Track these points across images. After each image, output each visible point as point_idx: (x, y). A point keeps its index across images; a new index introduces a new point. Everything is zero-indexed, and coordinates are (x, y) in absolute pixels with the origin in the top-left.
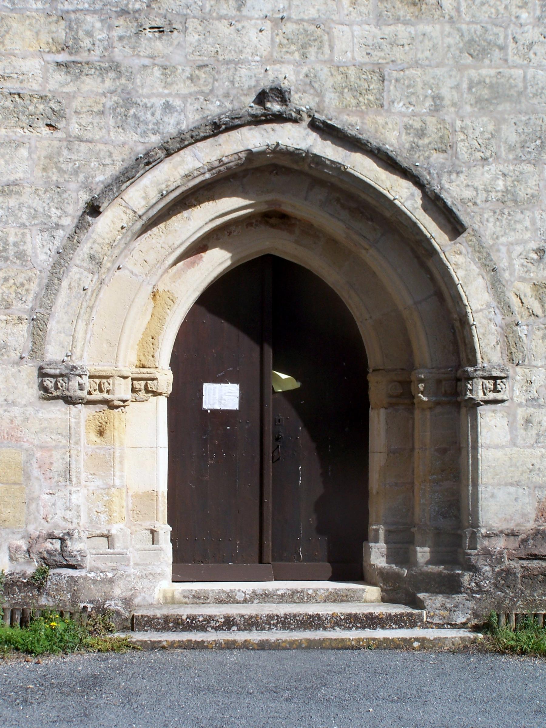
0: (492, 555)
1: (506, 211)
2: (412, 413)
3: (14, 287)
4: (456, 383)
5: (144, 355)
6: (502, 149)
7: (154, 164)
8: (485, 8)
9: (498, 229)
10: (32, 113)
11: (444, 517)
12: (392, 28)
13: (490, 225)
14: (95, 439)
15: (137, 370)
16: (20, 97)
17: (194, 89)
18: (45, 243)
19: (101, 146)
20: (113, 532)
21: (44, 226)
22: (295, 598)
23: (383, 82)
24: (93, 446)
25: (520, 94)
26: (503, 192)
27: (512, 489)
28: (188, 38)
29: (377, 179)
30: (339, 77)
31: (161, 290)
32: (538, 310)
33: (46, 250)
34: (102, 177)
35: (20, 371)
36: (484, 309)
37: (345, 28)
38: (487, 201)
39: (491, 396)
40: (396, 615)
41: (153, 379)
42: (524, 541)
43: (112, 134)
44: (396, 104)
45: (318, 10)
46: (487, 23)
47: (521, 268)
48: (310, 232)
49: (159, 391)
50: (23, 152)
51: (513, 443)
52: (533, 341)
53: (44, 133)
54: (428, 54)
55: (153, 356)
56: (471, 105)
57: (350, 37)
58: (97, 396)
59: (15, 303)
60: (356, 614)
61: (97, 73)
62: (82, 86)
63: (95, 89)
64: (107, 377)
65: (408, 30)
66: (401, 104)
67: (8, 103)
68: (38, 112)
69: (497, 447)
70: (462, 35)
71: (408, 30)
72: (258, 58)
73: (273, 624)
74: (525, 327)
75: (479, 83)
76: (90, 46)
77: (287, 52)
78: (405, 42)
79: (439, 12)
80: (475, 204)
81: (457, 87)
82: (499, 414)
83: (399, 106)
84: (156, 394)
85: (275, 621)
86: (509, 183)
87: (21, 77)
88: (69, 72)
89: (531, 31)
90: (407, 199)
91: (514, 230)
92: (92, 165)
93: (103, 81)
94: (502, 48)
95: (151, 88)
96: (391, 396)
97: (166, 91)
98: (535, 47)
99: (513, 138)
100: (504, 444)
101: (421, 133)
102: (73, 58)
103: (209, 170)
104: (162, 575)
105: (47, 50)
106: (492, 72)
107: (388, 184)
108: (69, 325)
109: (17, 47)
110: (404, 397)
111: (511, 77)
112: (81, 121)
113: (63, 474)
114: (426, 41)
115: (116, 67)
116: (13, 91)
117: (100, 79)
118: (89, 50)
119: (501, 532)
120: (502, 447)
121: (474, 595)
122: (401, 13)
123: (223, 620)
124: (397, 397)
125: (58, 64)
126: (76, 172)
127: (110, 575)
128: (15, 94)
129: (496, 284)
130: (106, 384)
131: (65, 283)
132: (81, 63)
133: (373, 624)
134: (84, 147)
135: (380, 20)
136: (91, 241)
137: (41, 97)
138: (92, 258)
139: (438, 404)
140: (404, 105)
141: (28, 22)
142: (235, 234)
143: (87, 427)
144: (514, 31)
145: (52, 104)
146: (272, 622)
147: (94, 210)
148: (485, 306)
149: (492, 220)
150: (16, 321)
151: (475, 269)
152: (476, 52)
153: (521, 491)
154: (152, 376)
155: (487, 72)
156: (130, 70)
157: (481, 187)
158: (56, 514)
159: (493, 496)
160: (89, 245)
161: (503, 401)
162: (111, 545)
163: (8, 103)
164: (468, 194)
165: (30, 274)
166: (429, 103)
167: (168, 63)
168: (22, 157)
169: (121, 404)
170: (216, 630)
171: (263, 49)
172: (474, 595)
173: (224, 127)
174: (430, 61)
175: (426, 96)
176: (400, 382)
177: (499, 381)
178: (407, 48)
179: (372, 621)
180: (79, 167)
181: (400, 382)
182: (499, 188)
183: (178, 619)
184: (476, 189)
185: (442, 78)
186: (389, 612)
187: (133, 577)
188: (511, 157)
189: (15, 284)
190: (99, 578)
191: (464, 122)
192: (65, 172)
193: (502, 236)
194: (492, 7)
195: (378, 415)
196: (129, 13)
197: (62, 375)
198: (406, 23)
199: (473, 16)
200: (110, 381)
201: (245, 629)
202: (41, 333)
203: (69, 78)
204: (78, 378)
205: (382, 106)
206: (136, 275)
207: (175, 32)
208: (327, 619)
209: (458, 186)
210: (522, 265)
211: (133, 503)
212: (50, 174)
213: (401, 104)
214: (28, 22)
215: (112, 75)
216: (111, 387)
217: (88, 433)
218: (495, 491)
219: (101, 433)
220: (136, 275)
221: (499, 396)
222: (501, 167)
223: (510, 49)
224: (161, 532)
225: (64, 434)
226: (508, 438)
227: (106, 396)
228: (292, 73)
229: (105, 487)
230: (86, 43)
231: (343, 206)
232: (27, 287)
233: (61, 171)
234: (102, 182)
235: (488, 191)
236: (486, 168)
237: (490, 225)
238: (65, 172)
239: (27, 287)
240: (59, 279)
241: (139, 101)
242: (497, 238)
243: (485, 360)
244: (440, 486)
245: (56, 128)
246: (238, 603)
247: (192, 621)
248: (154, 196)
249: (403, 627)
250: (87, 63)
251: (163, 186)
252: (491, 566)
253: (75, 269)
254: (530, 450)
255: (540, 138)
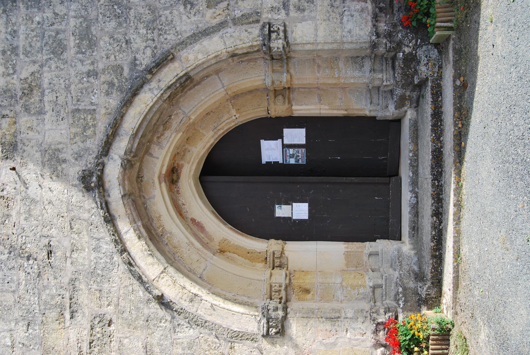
0: (391, 32)
1: (160, 27)
2: (295, 88)
3: (211, 351)
4: (275, 59)
5: (259, 258)
6: (120, 30)
7: (131, 259)
8: (33, 44)
9: (171, 32)
10: (101, 335)
11: (363, 66)
12: (46, 104)
13: (169, 37)
14: (311, 294)
15: (268, 263)
16: (92, 342)
17: (85, 233)
18: (183, 330)
19: (121, 292)
20: (371, 284)
21: (172, 331)
22: (415, 164)
23: (79, 110)
24: (316, 296)
25: (85, 19)
26: (147, 30)
27: (345, 19)
28: (54, 235)
29: (140, 113)
30: (77, 138)
31: (219, 248)
32: (225, 4)
33: (187, 330)
34: (141, 293)
35: (265, 349)
36: (224, 40)
37: (47, 135)
38: (154, 40)
39: (282, 34)
40: (433, 98)
41: (274, 253)
42: (381, 10)
43: (114, 285)
44: (93, 101)
45: (36, 152)
46: (42, 43)
47: (197, 16)
48: (179, 154)
49: (281, 250)
50: (126, 341)
51: (313, 19)
52: (245, 7)
53: (113, 328)
54: (62, 81)
55: (260, 253)
56: (93, 52)
57: (52, 131)
58: (283, 294)
59: (221, 351)
60: (432, 126)
61: (76, 293)
62: (84, 303)
63: (86, 295)
64: (271, 287)
65: (47, 94)
66: (93, 98)
67: (96, 350)
68: (101, 332)
69: (316, 30)
70: (50, 59)
71: (47, 94)
72: (66, 191)
73: (438, 183)
74: (236, 12)
75: (79, 47)
76: (60, 297)
77: (62, 172)
78: (55, 95)
79: (36, 75)
80: (155, 48)
81: (82, 61)
82: (294, 29)
83: (94, 100)
84: (282, 253)
85: (436, 182)
86: (142, 26)
87: (80, 341)
88: (76, 311)
89: (46, 14)
90: (153, 93)
91: (172, 21)
92: (133, 298)
93: (82, 290)
94: (58, 33)
95: (85, 258)
96: (284, 103)
97: (87, 250)
98: (56, 11)
99: (113, 24)
100: (314, 25)
101: (111, 84)
102: (68, 308)
103: (135, 223)
104: (399, 250)
105: (63, 324)
106: (72, 38)
107: (143, 106)
108: (235, 317)
109: (61, 342)
110: (284, 92)
111: (75, 26)
112: (106, 305)
113: (333, 323)
114: (54, 82)
115: (73, 281)
116: (89, 347)
117: (80, 292)
118: (63, 298)
119: (374, 25)
120: (316, 26)
121: (418, 44)
122: (37, 99)
123: (435, 218)
124: (284, 98)
125: (72, 318)
126: (138, 309)
127: (401, 290)
128: (90, 346)
129: (206, 33)
130: (276, 288)
131: (208, 318)
132: (71, 304)
133: (439, 114)
134: (122, 303)
135: (41, 112)
136: (180, 300)
137: (92, 329)
138: (191, 301)
139: (288, 71)
140: (93, 96)
141: (47, 335)
142: (184, 201)
143: (303, 300)
144: (47, 25)
145: (96, 323)
146: (437, 184)
147: (161, 300)
148: (222, 40)
149: (165, 36)
150: (233, 350)
151: (197, 47)
152: (60, 49)
153: (346, 13)
154: (272, 254)
155: (72, 42)
156: (74, 273)
157: (144, 44)
158: (360, 328)
159: (350, 32)
160: (183, 302)
161: (285, 26)
162: (380, 286)
163: (96, 350)
164: (149, 52)
165: (202, 340)
166: (91, 79)
167: (70, 248)
168: (128, 344)
169: (288, 278)
170: (442, 222)
171: (60, 187)
172: (418, 44)
173: (107, 214)
174: (66, 79)
175: (88, 81)
176: (275, 97)
177: (272, 29)
178: (58, 95)
179: (437, 115)
180: (135, 307)
181: (275, 97)
182: (145, 32)
183: (434, 249)
184: (146, 47)
185: (76, 72)
186: (430, 103)
187: (401, 272)
188: (125, 25)
189: (209, 351)
190: (403, 298)
191: (104, 56)
192: (138, 316)
193: (176, 29)
194: (32, 40)
195: (296, 110)
196: (40, 272)
197: (268, 322)
198: (43, 94)
199: (38, 52)
200: (273, 285)
201: (441, 202)
202: (240, 335)
203: (80, 311)
204: (270, 312)
205: (94, 110)
206: (206, 267)
207: (51, 243)
208: (435, 146)
209: (144, 59)
210: (195, 15)
211: (352, 267)
212: (139, 325)
213: (93, 98)
214: (47, 335)
215: (77, 283)
216: (278, 285)
217: (306, 300)
218: (346, 30)
219: (307, 291)
220: (206, 267)
221: (282, 28)
222: (132, 31)
223: (58, 27)
224: (371, 250)
225: (307, 321)
226: (310, 22)
227: (283, 288)
228: (75, 169)
229: (342, 289)
230: (58, 299)
231: (162, 135)
232: (210, 343)
233: (136, 319)
234: (144, 292)
235: (147, 39)
236: (132, 41)
237: (169, 37)
238: (138, 316)
239: (210, 343)
240: (206, 322)
241: (93, 267)
242: (177, 32)
243: (258, 39)
244: (342, 69)
245: (111, 320)
246: (418, 202)
247: (435, 239)
248: (150, 260)
249: (441, 93)
250: (71, 299)
251: (145, 253)
252: (398, 32)
253: (199, 312)
254: (318, 7)
255: (113, 6)
